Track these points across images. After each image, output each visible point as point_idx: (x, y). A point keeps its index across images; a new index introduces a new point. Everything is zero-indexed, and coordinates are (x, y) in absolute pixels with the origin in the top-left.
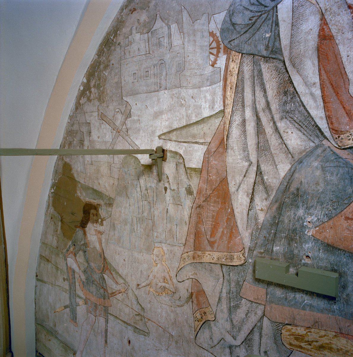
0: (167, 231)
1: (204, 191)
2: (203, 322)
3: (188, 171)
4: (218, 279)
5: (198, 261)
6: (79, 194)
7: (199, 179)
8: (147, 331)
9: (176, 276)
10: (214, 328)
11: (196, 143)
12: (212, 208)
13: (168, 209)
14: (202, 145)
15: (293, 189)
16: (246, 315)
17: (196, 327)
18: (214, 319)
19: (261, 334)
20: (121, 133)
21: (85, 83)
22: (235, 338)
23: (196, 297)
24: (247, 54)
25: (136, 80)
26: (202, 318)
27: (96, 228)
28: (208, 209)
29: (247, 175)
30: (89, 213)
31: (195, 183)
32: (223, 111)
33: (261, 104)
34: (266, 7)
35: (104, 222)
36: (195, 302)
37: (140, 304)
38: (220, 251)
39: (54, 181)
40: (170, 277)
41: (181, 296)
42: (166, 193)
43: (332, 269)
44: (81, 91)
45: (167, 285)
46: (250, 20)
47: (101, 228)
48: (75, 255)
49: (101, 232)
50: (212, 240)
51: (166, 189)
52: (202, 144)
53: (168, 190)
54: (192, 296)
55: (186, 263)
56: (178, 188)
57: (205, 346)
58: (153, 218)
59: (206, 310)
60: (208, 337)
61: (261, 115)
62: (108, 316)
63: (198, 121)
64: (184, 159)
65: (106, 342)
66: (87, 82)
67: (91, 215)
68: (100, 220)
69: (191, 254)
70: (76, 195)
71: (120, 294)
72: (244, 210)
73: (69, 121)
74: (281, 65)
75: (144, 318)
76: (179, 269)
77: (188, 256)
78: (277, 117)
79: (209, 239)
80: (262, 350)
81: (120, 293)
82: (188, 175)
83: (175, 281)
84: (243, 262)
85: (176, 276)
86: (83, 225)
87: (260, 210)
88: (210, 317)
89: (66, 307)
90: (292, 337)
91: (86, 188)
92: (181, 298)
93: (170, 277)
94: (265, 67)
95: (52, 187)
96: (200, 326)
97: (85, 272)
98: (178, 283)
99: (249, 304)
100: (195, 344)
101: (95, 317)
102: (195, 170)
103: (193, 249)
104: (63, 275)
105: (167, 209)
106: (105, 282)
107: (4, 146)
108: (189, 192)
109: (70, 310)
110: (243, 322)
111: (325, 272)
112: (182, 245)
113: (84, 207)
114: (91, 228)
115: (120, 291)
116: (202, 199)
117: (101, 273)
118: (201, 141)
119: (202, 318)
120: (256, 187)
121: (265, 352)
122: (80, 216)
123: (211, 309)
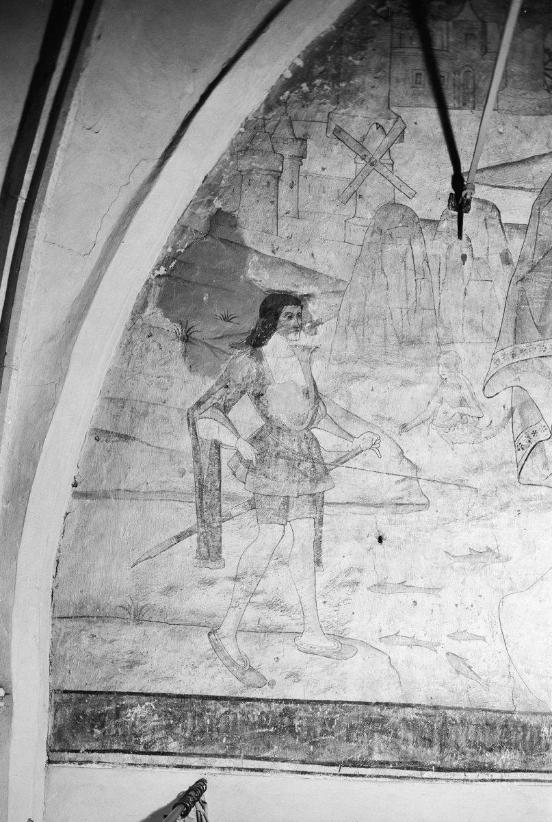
0: (465, 324)
1: (531, 257)
3: (507, 229)
5: (521, 359)
7: (522, 241)
9: (484, 390)
11: (522, 188)
13: (468, 289)
14: (530, 191)
21: (299, 67)
26: (529, 441)
27: (294, 343)
28: (536, 281)
37: (408, 460)
38: (100, 697)
39: (170, 250)
40: (473, 394)
42: (464, 264)
44: (286, 79)
49: (310, 349)
50: (542, 324)
51: (464, 257)
52: (530, 190)
53: (469, 259)
54: (512, 414)
56: (487, 255)
58: (437, 307)
63: (523, 160)
64: (499, 212)
66: (304, 66)
70: (242, 277)
73: (242, 130)
79: (537, 324)
82: (506, 234)
85: (484, 390)
86: (256, 341)
92: (493, 422)
98: (489, 399)
102: (516, 227)
103: (512, 343)
105: (466, 289)
108: (506, 260)
111: (245, 761)
112: (493, 340)
113: (265, 300)
114: (276, 344)
116: (527, 269)
118: (529, 186)
119: (529, 441)
122: (250, 322)
123: (544, 424)
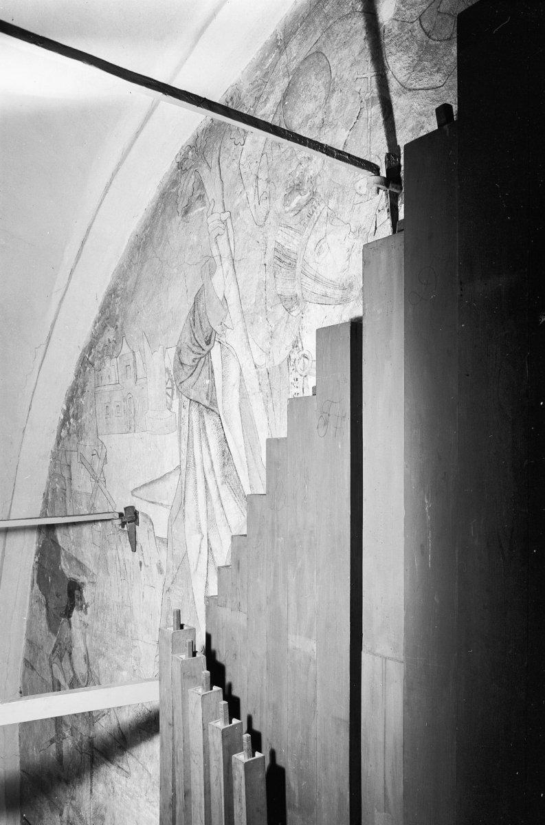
6: (63, 567)
20: (100, 484)
24: (194, 401)
25: (109, 416)
32: (179, 467)
33: (207, 466)
34: (203, 349)
35: (88, 609)
43: (415, 48)
46: (193, 361)
61: (207, 473)
68: (84, 606)
71: (104, 718)
72: (391, 664)
74: (218, 420)
78: (219, 483)
81: (104, 715)
86: (68, 614)
87: (206, 597)
89: (52, 741)
91: (71, 558)
94: (207, 417)
95: (37, 554)
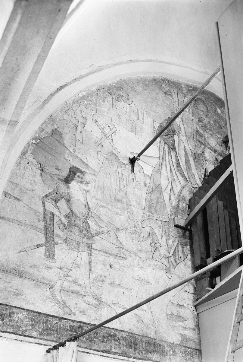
2: (156, 247)
4: (161, 227)
8: (125, 257)
10: (161, 251)
12: (154, 197)
15: (182, 196)
16: (173, 243)
17: (152, 251)
18: (160, 246)
19: (178, 250)
22: (169, 253)
23: (152, 236)
29: (168, 186)
30: (75, 175)
31: (148, 181)
33: (171, 164)
36: (151, 238)
41: (54, 288)
45: (136, 229)
47: (87, 188)
48: (56, 202)
55: (145, 219)
57: (157, 259)
59: (157, 242)
60: (158, 255)
62: (91, 251)
65: (90, 270)
67: (76, 176)
69: (147, 214)
75: (123, 249)
76: (142, 221)
77: (146, 215)
80: (179, 256)
81: (103, 234)
83: (140, 227)
84: (169, 220)
88: (158, 245)
90: (187, 250)
93: (138, 225)
96: (154, 250)
97: (67, 216)
99: (173, 238)
100: (153, 259)
101: (77, 253)
104: (38, 216)
106: (89, 226)
107: (2, 215)
109: (46, 249)
110: (172, 246)
115: (103, 232)
117: (85, 219)
120: (171, 191)
121: (180, 257)
122: (65, 173)
